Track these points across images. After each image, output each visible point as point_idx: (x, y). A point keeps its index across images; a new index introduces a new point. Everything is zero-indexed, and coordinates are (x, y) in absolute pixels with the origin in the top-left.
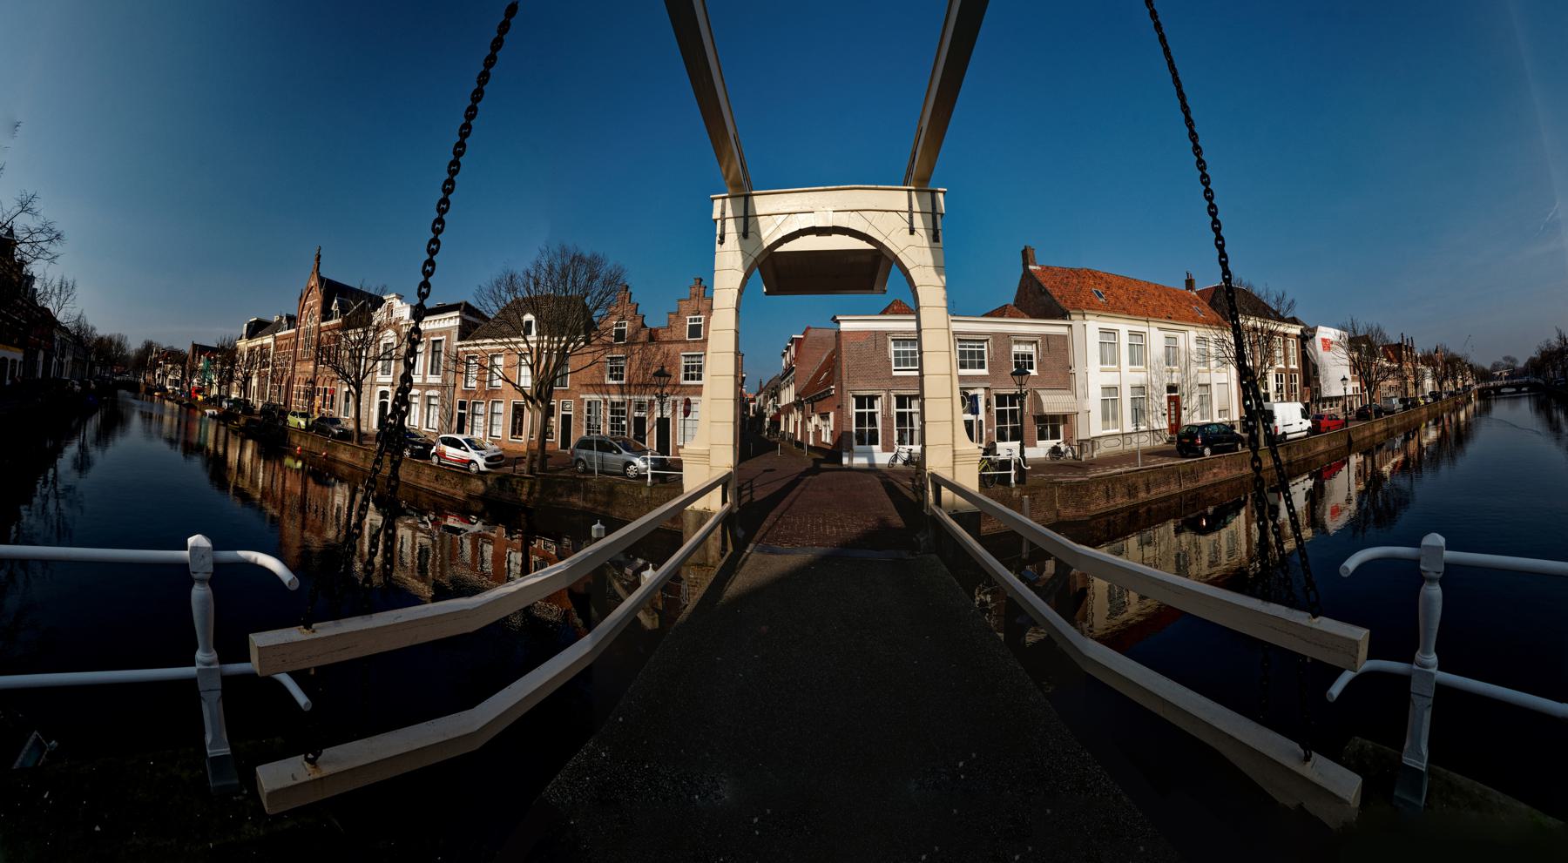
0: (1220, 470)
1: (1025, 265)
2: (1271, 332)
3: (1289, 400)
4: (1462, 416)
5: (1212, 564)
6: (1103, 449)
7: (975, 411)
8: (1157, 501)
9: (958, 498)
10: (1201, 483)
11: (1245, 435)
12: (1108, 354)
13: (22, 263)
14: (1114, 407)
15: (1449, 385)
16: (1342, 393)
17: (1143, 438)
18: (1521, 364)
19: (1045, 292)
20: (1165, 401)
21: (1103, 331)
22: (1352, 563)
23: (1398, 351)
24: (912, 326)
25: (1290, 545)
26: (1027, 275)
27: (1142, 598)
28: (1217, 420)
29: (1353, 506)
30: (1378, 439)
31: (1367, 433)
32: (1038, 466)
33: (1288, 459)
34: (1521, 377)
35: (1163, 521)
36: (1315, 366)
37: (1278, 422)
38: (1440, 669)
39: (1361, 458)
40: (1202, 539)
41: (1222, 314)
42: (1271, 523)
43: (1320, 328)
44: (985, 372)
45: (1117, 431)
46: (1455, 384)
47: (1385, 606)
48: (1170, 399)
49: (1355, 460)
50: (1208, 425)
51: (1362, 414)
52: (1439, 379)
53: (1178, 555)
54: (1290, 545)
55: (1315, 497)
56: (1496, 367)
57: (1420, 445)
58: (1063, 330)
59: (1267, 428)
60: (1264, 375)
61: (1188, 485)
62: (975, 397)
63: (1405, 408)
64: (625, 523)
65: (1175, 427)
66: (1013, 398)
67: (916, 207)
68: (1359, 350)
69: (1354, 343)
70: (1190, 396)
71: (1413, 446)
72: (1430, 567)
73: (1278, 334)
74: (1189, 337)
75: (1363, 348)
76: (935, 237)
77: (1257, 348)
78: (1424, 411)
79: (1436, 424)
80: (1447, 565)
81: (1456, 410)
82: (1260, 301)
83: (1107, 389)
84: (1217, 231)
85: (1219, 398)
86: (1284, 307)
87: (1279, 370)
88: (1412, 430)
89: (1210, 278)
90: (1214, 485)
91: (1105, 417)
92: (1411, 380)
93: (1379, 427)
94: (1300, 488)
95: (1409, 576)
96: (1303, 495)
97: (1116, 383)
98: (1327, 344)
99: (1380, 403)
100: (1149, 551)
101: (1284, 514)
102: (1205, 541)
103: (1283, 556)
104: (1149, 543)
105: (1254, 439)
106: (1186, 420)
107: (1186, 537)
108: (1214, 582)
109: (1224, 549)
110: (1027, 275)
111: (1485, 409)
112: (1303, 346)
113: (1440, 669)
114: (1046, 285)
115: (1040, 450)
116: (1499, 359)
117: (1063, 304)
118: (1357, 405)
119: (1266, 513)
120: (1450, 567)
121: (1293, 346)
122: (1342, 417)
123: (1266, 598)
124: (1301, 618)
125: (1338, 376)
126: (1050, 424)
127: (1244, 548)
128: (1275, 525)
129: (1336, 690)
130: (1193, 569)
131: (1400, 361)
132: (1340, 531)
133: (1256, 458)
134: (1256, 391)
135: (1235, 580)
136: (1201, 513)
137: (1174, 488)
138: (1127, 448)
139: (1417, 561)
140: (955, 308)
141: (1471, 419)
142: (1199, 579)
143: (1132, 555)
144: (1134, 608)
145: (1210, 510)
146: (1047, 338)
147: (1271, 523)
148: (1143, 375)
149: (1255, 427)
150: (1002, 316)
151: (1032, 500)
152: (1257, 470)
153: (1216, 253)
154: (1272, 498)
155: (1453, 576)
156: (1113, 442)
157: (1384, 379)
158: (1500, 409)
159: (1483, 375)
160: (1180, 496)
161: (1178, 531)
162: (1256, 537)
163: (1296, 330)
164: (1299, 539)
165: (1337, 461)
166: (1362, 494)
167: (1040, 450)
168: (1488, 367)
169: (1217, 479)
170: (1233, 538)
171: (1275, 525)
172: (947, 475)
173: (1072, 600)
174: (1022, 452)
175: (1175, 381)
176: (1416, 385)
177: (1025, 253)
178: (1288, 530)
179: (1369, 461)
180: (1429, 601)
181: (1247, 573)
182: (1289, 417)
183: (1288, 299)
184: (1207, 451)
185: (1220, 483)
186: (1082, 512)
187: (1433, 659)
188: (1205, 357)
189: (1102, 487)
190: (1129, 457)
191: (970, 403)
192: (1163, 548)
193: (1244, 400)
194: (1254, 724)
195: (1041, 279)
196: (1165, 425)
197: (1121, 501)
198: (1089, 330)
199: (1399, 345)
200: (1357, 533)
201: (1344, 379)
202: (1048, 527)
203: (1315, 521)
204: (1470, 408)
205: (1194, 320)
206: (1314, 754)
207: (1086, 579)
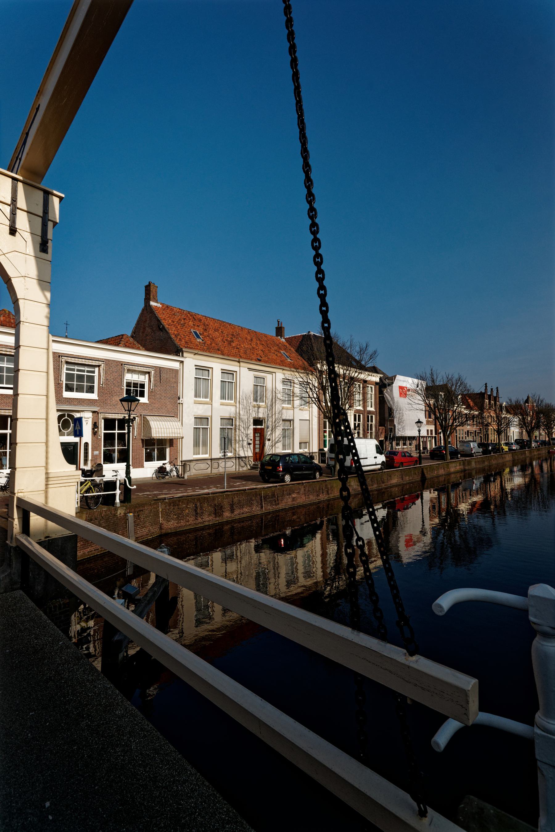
0: (297, 495)
1: (147, 299)
2: (352, 379)
3: (365, 437)
5: (289, 583)
6: (193, 472)
7: (79, 433)
8: (240, 521)
9: (51, 524)
10: (281, 506)
12: (202, 389)
13: (399, 538)
14: (205, 435)
15: (541, 434)
16: (416, 434)
17: (230, 464)
19: (162, 329)
20: (251, 432)
21: (199, 368)
22: (446, 601)
23: (478, 400)
24: (10, 340)
26: (147, 309)
27: (225, 611)
28: (297, 450)
29: (428, 539)
32: (144, 485)
33: (364, 491)
35: (247, 539)
36: (391, 410)
43: (399, 377)
44: (94, 396)
45: (207, 456)
48: (255, 430)
49: (428, 495)
50: (289, 455)
51: (436, 454)
57: (503, 489)
58: (175, 365)
61: (269, 508)
62: (80, 420)
63: (484, 452)
65: (259, 455)
66: (122, 423)
67: (22, 202)
69: (430, 391)
70: (274, 429)
71: (494, 489)
73: (358, 380)
74: (276, 379)
76: (43, 246)
78: (509, 457)
82: (344, 351)
84: (320, 280)
85: (303, 429)
86: (366, 357)
87: (357, 411)
88: (491, 474)
91: (196, 444)
93: (455, 467)
97: (208, 414)
98: (404, 392)
99: (455, 445)
100: (232, 567)
106: (269, 450)
107: (265, 556)
110: (147, 309)
112: (381, 392)
114: (165, 323)
115: (146, 471)
117: (177, 342)
118: (431, 445)
121: (371, 392)
122: (415, 455)
124: (396, 653)
125: (412, 417)
126: (156, 447)
129: (442, 738)
130: (271, 588)
131: (481, 409)
132: (415, 564)
135: (310, 600)
136: (279, 533)
137: (256, 510)
138: (215, 471)
140: (58, 327)
143: (216, 570)
145: (288, 532)
146: (160, 370)
148: (233, 409)
150: (117, 345)
151: (137, 517)
156: (203, 466)
157: (462, 424)
161: (258, 549)
163: (376, 378)
165: (411, 495)
167: (146, 471)
169: (296, 503)
170: (309, 558)
172: (37, 500)
173: (163, 608)
174: (128, 472)
175: (261, 416)
176: (499, 432)
177: (148, 288)
179: (443, 498)
182: (368, 451)
183: (370, 350)
184: (287, 478)
185: (299, 507)
186: (183, 523)
188: (290, 397)
189: (191, 505)
190: (217, 480)
191: (69, 422)
194: (353, 761)
195: (160, 316)
196: (250, 454)
197: (208, 519)
201: (419, 422)
202: (142, 543)
205: (282, 364)
206: (429, 809)
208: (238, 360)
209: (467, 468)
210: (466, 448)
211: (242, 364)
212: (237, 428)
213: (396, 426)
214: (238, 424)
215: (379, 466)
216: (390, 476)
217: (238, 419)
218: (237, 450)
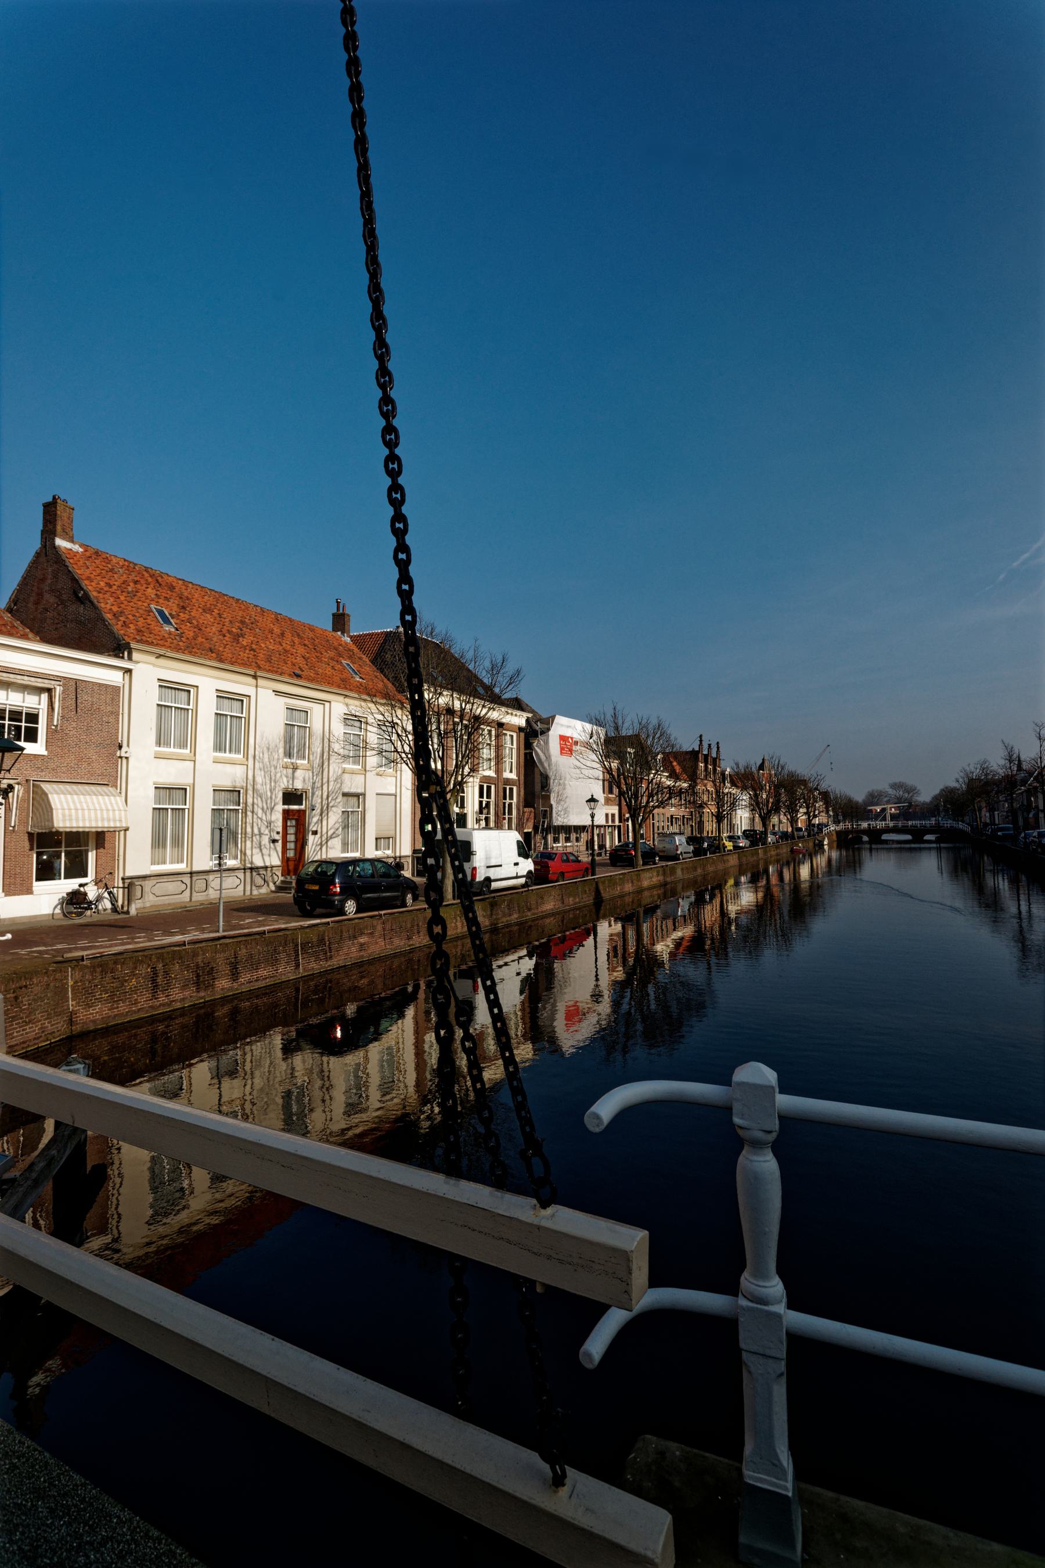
0: (372, 940)
2: (477, 719)
3: (499, 826)
4: (805, 872)
8: (252, 994)
10: (336, 962)
11: (420, 881)
14: (179, 823)
15: (781, 822)
16: (586, 821)
18: (926, 795)
19: (85, 599)
20: (277, 817)
21: (166, 686)
22: (607, 1107)
23: (689, 763)
25: (493, 1073)
27: (217, 1179)
28: (371, 853)
29: (605, 1007)
30: (647, 898)
31: (628, 887)
33: (491, 923)
34: (923, 817)
35: (262, 1031)
36: (545, 779)
37: (479, 860)
38: (790, 1306)
39: (618, 927)
40: (336, 1065)
41: (395, 680)
42: (459, 1033)
43: (559, 719)
45: (182, 867)
46: (793, 821)
47: (673, 1183)
48: (287, 814)
49: (607, 929)
50: (355, 862)
51: (621, 857)
52: (763, 811)
53: (288, 1095)
54: (493, 1073)
55: (538, 987)
56: (874, 798)
57: (723, 913)
58: (115, 678)
59: (458, 870)
60: (460, 786)
61: (312, 966)
63: (698, 852)
65: (293, 863)
68: (621, 757)
69: (613, 746)
70: (324, 812)
71: (710, 914)
73: (489, 722)
74: (331, 713)
75: (628, 757)
77: (451, 742)
78: (733, 861)
79: (754, 880)
80: (782, 1118)
81: (794, 860)
82: (463, 667)
83: (165, 791)
85: (378, 816)
86: (502, 680)
89: (380, 617)
90: (359, 965)
91: (158, 841)
92: (711, 809)
93: (650, 878)
94: (512, 972)
95: (715, 1136)
96: (517, 983)
97: (185, 780)
98: (567, 745)
99: (651, 841)
100: (232, 1089)
101: (482, 1016)
102: (340, 1067)
103: (481, 1093)
104: (232, 1073)
105: (435, 887)
106: (314, 852)
107: (303, 1061)
108: (356, 1143)
109: (375, 1080)
111: (851, 864)
112: (528, 746)
113: (790, 1306)
114: (90, 588)
116: (882, 785)
117: (118, 628)
118: (612, 841)
119: (450, 1015)
120: (791, 1125)
121: (511, 745)
122: (585, 858)
123: (453, 1171)
124: (520, 1208)
125: (581, 792)
127: (411, 1077)
128: (467, 1036)
129: (596, 1345)
130: (316, 1120)
131: (693, 778)
132: (583, 1050)
133: (437, 919)
134: (444, 809)
135: (394, 1139)
136: (329, 1017)
137: (285, 971)
138: (198, 897)
139: (727, 1110)
141: (821, 879)
142: (326, 1137)
143: (196, 1096)
144: (201, 1199)
145: (351, 1009)
146: (75, 687)
147: (459, 1033)
149: (438, 867)
152: (438, 939)
153: (395, 573)
154: (461, 987)
155: (793, 1139)
156: (172, 887)
157: (662, 804)
158: (878, 867)
159: (846, 809)
160: (295, 984)
162: (433, 1056)
163: (518, 719)
164: (509, 1061)
165: (576, 930)
166: (619, 988)
168: (859, 797)
169: (365, 955)
170: (392, 1059)
171: (467, 1036)
175: (299, 785)
176: (719, 818)
178: (491, 1045)
179: (631, 933)
180: (756, 1180)
181: (416, 1124)
182: (497, 854)
183: (510, 668)
184: (350, 906)
185: (372, 962)
187: (775, 1287)
188: (358, 749)
189: (144, 970)
192: (258, 1082)
193: (423, 823)
195: (79, 572)
197: (180, 995)
198: (145, 679)
199: (694, 755)
200: (617, 1049)
201: (592, 800)
203: (538, 1031)
204: (821, 861)
205: (343, 685)
207: (105, 1146)
208: (252, 673)
209: (668, 879)
210: (668, 846)
211: (261, 682)
212: (249, 808)
213: (554, 806)
215: (523, 881)
216: (542, 898)
217: (250, 792)
218: (249, 852)
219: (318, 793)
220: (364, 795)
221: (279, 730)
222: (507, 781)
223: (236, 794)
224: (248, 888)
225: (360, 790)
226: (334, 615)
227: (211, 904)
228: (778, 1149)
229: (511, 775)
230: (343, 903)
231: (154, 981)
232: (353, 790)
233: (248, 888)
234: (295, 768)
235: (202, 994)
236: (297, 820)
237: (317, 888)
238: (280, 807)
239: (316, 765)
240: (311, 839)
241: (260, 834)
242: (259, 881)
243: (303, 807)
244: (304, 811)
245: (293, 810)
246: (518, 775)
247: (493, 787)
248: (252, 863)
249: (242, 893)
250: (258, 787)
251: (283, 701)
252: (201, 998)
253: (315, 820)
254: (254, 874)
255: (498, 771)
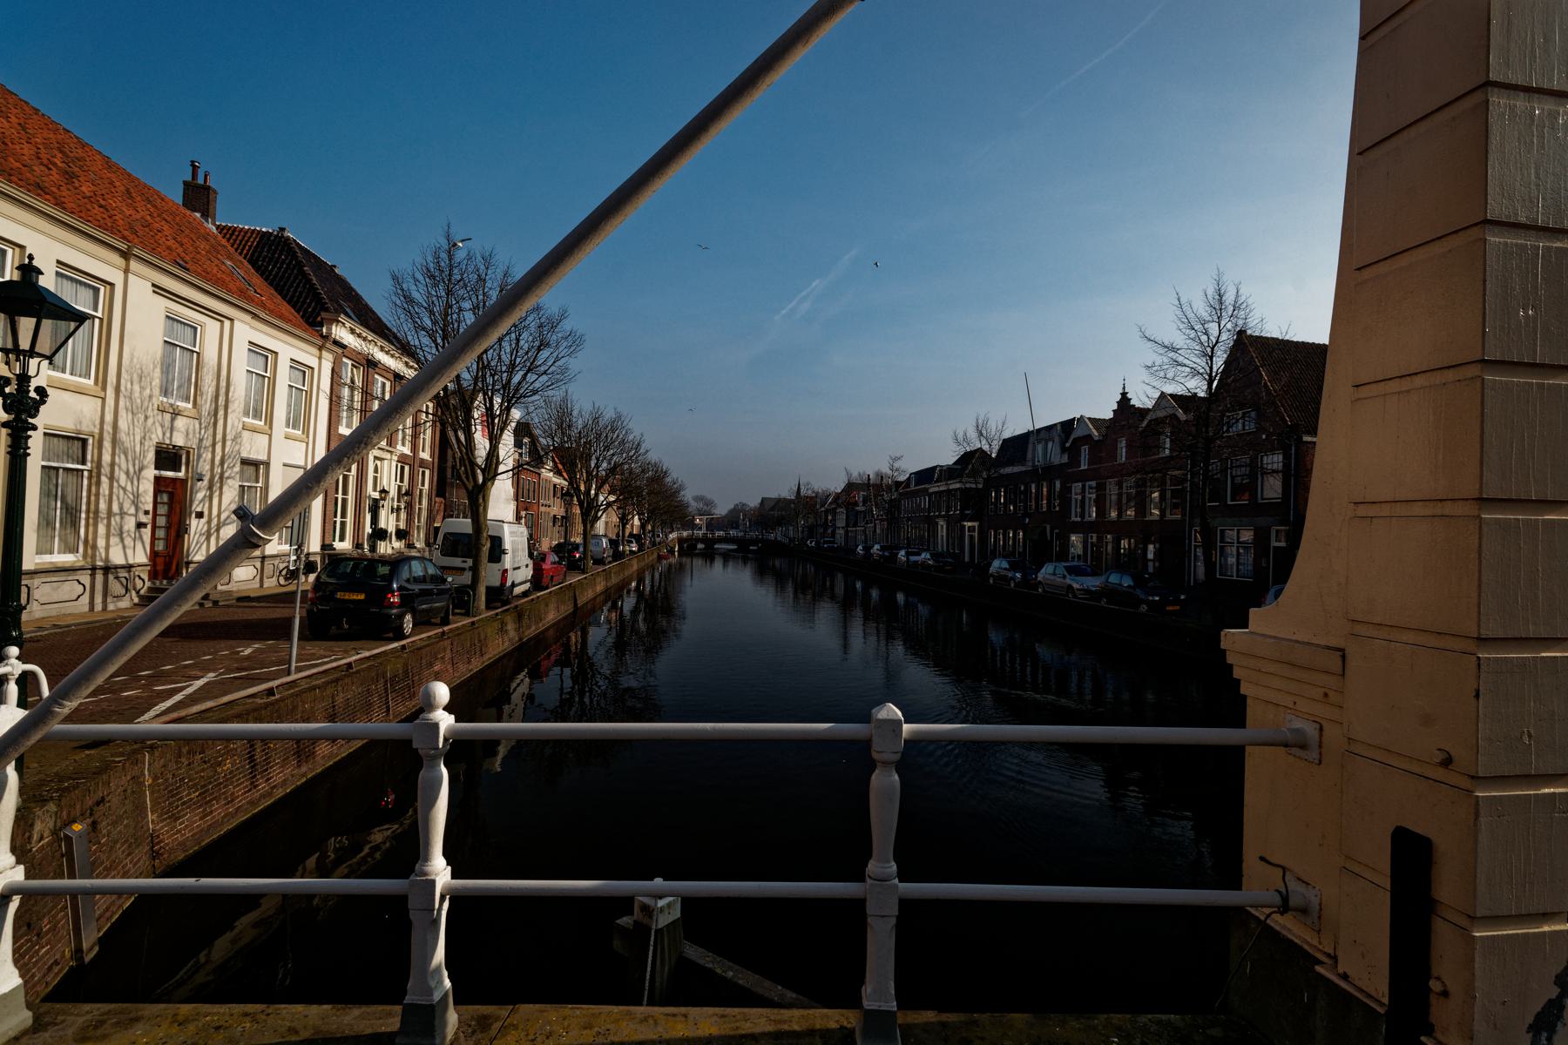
18: (721, 510)
20: (147, 487)
64: (163, 634)
70: (216, 484)
72: (884, 750)
113: (903, 877)
155: (914, 755)
175: (179, 440)
183: (567, 325)
196: (140, 556)
208: (123, 247)
211: (134, 265)
212: (106, 470)
214: (106, 458)
217: (107, 445)
218: (101, 543)
219: (207, 456)
220: (267, 464)
221: (157, 349)
222: (423, 463)
223: (78, 444)
224: (98, 599)
225: (263, 457)
226: (185, 183)
227: (41, 628)
228: (900, 767)
229: (425, 455)
230: (401, 617)
231: (251, 759)
232: (253, 456)
233: (98, 599)
234: (176, 413)
235: (304, 769)
236: (171, 496)
237: (362, 597)
238: (151, 473)
239: (205, 413)
240: (196, 526)
241: (122, 514)
242: (116, 588)
243: (181, 474)
244: (184, 482)
245: (166, 479)
246: (432, 455)
247: (407, 468)
248: (107, 559)
249: (86, 609)
250: (122, 436)
251: (163, 303)
252: (304, 775)
253: (200, 496)
254: (111, 577)
255: (414, 448)
